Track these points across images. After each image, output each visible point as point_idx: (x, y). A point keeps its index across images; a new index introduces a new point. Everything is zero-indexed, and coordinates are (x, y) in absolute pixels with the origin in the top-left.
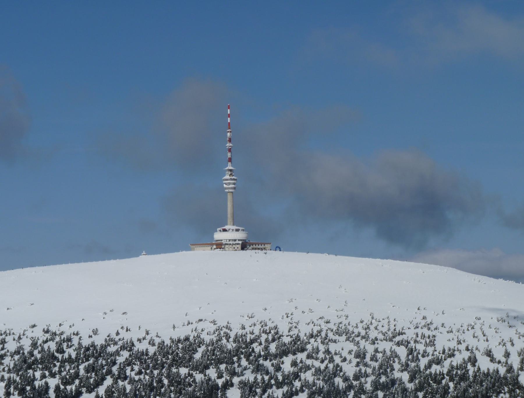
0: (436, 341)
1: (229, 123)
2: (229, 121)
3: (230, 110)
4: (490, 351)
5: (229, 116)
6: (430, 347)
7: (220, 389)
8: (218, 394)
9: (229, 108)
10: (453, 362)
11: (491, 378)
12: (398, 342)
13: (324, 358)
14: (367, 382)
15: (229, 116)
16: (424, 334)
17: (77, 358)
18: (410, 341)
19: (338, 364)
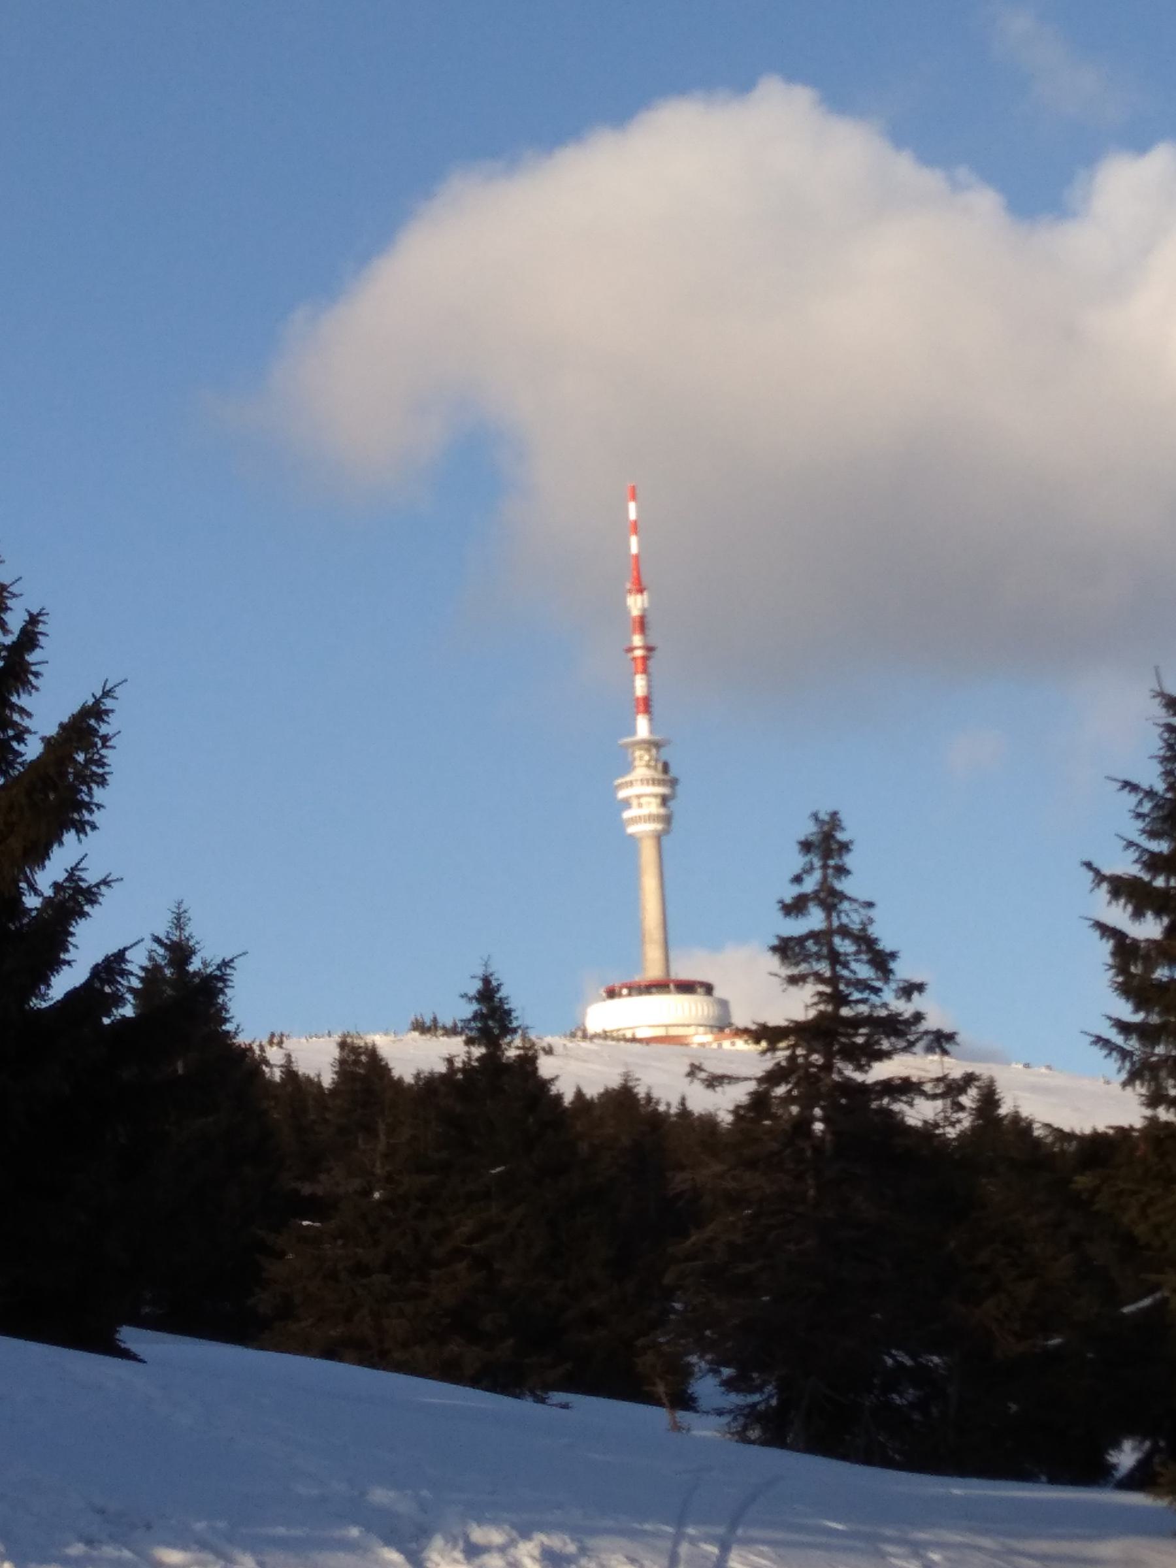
0: (85, 922)
1: (637, 557)
2: (634, 549)
3: (629, 548)
4: (1158, 667)
5: (635, 527)
6: (99, 794)
7: (849, 1040)
8: (494, 1169)
9: (634, 497)
10: (788, 901)
11: (797, 944)
12: (738, 1390)
13: (828, 990)
14: (110, 886)
15: (635, 527)
16: (638, 1085)
17: (833, 981)
18: (268, 1049)
19: (923, 1018)
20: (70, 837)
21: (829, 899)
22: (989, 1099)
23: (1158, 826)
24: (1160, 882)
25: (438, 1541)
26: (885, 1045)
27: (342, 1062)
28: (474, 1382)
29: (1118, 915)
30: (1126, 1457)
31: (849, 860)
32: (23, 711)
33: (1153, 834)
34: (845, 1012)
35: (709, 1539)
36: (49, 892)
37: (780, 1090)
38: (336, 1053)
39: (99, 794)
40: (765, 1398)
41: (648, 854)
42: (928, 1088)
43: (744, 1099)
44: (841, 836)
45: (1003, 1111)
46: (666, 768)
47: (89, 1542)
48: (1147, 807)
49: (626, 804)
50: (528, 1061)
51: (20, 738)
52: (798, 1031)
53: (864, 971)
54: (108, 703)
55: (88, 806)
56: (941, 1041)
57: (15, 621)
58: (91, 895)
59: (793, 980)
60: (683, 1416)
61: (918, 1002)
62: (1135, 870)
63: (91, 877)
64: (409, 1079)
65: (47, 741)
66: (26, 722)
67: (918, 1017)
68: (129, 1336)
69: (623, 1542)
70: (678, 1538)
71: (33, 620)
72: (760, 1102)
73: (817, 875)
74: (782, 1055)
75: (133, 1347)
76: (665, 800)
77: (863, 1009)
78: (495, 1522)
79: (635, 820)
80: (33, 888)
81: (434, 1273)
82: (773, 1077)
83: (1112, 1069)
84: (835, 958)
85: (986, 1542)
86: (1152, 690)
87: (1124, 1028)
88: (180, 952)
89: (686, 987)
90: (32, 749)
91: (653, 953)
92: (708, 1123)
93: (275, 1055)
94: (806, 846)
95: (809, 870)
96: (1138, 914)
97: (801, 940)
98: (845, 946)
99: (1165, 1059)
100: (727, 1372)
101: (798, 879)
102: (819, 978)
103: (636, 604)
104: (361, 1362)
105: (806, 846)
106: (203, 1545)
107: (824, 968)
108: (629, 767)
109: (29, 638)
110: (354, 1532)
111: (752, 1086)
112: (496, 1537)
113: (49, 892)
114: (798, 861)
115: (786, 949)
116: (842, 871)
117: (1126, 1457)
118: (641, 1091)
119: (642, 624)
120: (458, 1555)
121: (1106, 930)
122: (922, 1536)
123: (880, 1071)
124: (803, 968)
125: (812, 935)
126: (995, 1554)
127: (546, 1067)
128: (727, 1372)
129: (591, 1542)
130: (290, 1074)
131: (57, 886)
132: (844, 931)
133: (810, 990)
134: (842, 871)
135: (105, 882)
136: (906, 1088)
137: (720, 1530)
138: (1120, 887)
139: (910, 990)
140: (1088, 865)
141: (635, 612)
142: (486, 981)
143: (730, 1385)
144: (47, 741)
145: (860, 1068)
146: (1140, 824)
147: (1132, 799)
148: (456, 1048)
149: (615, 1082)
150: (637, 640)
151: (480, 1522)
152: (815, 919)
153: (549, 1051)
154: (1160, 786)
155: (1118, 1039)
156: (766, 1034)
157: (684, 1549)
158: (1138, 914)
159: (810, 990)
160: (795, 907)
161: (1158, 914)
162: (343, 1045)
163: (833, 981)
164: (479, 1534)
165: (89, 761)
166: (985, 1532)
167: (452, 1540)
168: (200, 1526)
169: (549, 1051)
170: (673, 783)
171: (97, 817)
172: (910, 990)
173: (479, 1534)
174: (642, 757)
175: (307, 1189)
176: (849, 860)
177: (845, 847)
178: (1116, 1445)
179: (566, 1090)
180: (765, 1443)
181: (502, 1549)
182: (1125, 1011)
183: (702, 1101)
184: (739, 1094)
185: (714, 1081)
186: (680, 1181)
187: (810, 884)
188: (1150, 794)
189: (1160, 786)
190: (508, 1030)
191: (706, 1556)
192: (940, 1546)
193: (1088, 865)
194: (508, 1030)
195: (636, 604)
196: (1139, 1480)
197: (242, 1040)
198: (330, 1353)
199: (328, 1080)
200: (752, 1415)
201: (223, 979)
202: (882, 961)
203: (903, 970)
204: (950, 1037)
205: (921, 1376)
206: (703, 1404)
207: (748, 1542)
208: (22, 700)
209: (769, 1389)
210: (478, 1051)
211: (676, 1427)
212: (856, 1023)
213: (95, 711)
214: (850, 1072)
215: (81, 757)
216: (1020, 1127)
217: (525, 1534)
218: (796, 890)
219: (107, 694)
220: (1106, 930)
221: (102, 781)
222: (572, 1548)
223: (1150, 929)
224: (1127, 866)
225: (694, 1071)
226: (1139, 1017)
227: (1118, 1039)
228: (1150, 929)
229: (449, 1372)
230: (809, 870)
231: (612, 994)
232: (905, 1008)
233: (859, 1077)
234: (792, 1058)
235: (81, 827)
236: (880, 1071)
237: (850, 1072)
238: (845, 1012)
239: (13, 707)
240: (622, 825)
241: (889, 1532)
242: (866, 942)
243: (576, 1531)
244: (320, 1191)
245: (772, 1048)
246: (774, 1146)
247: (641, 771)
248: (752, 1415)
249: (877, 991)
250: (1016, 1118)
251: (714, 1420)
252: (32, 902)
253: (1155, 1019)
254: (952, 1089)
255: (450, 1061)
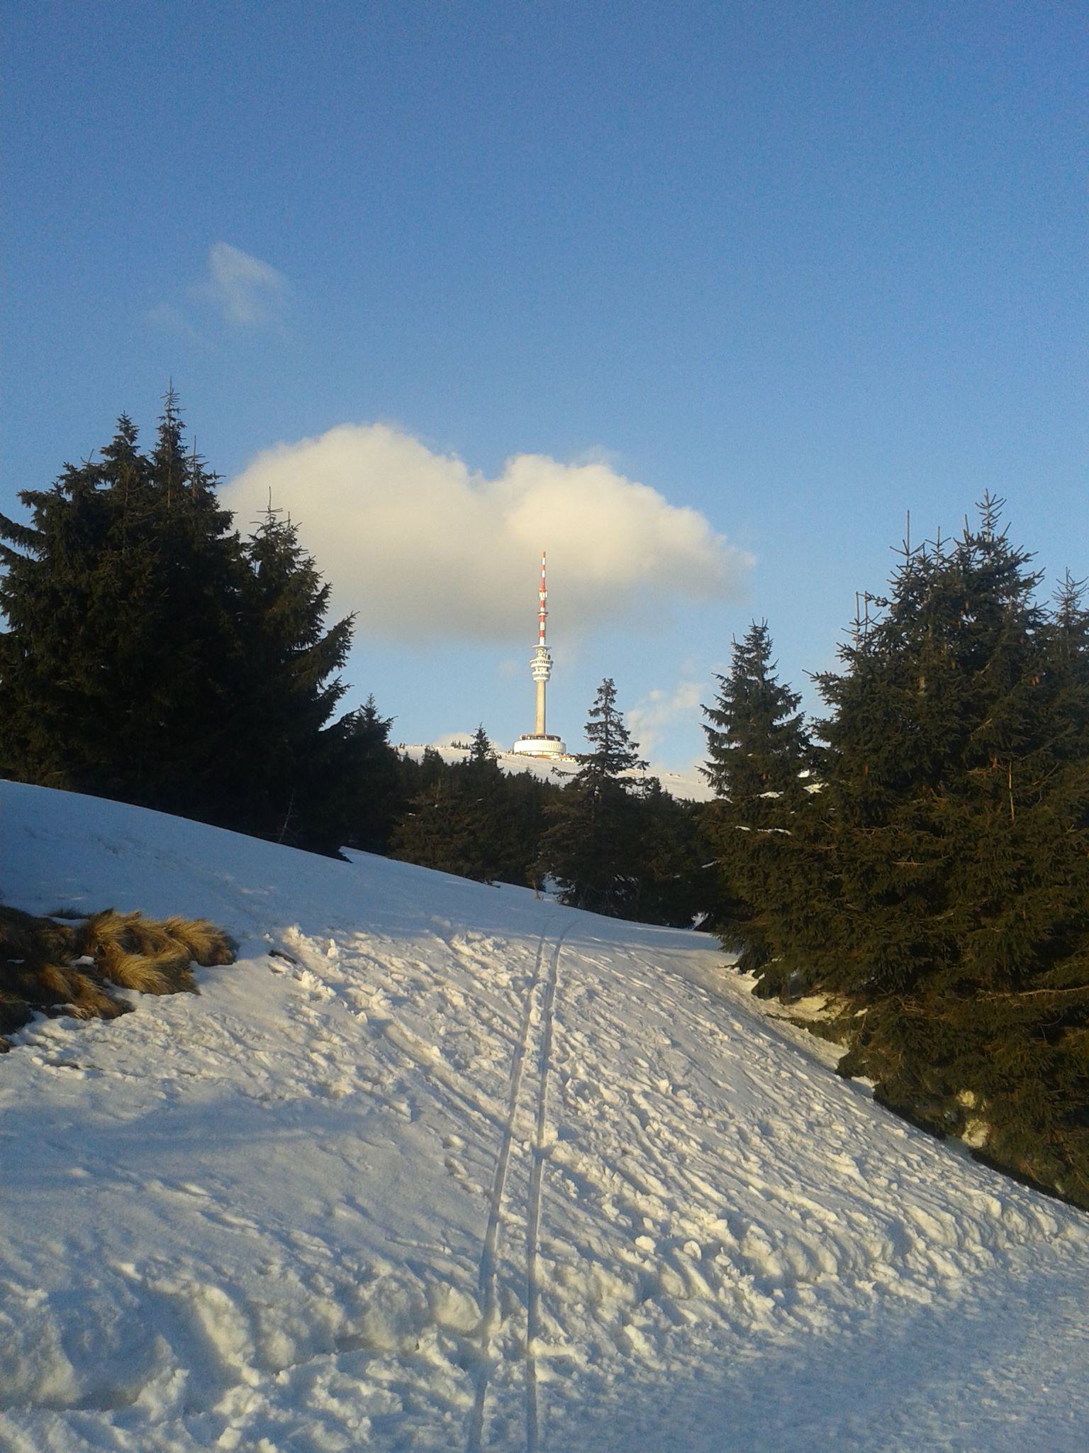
6: (347, 653)
17: (606, 740)
20: (336, 668)
21: (607, 710)
22: (658, 787)
23: (729, 692)
24: (728, 713)
25: (457, 937)
26: (624, 765)
27: (426, 756)
28: (467, 876)
29: (713, 724)
30: (699, 919)
31: (615, 697)
32: (321, 620)
33: (727, 695)
34: (610, 752)
35: (552, 942)
36: (327, 688)
37: (584, 779)
38: (424, 752)
39: (347, 653)
40: (572, 889)
41: (541, 687)
42: (638, 781)
43: (570, 781)
44: (613, 688)
45: (662, 791)
46: (549, 657)
47: (332, 928)
48: (726, 685)
49: (534, 669)
50: (494, 761)
51: (319, 631)
52: (593, 758)
53: (618, 738)
54: (352, 620)
55: (343, 657)
56: (644, 765)
57: (320, 587)
58: (342, 691)
59: (592, 739)
60: (541, 893)
61: (636, 751)
62: (719, 708)
63: (343, 684)
64: (450, 764)
65: (329, 632)
66: (322, 625)
67: (636, 756)
68: (344, 850)
69: (521, 941)
70: (541, 942)
71: (327, 587)
72: (576, 783)
73: (604, 701)
74: (586, 765)
75: (346, 855)
76: (548, 669)
77: (616, 751)
78: (477, 931)
79: (537, 675)
80: (321, 686)
81: (455, 836)
82: (582, 774)
83: (705, 781)
84: (607, 732)
85: (650, 949)
86: (68, 467)
87: (710, 765)
88: (371, 712)
89: (551, 738)
90: (323, 635)
91: (540, 724)
92: (556, 787)
93: (401, 751)
94: (600, 691)
95: (601, 699)
96: (719, 724)
97: (596, 725)
98: (612, 728)
99: (725, 777)
100: (558, 879)
101: (596, 703)
102: (601, 739)
103: (542, 596)
104: (426, 866)
105: (600, 691)
106: (373, 932)
107: (603, 735)
108: (537, 656)
109: (325, 593)
110: (427, 931)
111: (573, 777)
112: (478, 937)
113: (327, 688)
114: (598, 696)
115: (590, 728)
116: (612, 701)
117: (699, 919)
118: (533, 775)
119: (544, 604)
120: (464, 942)
121: (707, 728)
122: (626, 945)
123: (621, 774)
124: (596, 735)
125: (599, 723)
126: (654, 953)
127: (500, 764)
128: (558, 879)
129: (511, 940)
130: (407, 758)
131: (330, 686)
132: (612, 723)
133: (598, 743)
134: (612, 701)
135: (348, 686)
136: (630, 781)
137: (557, 939)
138: (714, 714)
139: (634, 746)
140: (703, 706)
141: (542, 599)
142: (480, 731)
143: (559, 883)
144: (329, 632)
145: (614, 773)
146: (723, 691)
147: (721, 682)
148: (467, 753)
149: (524, 771)
150: (542, 609)
151: (472, 930)
152: (601, 718)
153: (500, 758)
154: (731, 678)
155: (709, 770)
156: (581, 759)
157: (544, 945)
158: (719, 724)
159: (598, 743)
160: (594, 713)
161: (727, 724)
162: (426, 750)
163: (606, 740)
164: (471, 935)
165: (344, 641)
166: (650, 945)
167: (461, 937)
168: (372, 925)
169: (500, 758)
170: (552, 662)
171: (345, 662)
172: (634, 746)
173: (471, 935)
174: (541, 653)
175: (411, 802)
176: (615, 697)
177: (614, 692)
178: (696, 914)
179: (505, 772)
180: (568, 905)
181: (480, 941)
182: (712, 760)
183: (554, 779)
184: (569, 779)
185: (561, 774)
186: (547, 809)
187: (600, 705)
188: (727, 680)
189: (731, 678)
190: (486, 749)
191: (551, 948)
192: (634, 949)
193: (703, 706)
194: (486, 749)
195: (542, 596)
196: (701, 928)
197: (392, 745)
198: (416, 862)
199: (420, 762)
200: (566, 895)
201: (388, 725)
202: (624, 735)
203: (631, 738)
204: (647, 764)
205: (627, 885)
206: (547, 889)
207: (566, 944)
208: (321, 616)
209: (573, 886)
210: (475, 756)
211: (539, 897)
212: (614, 756)
213: (347, 622)
214: (610, 774)
215: (341, 639)
216: (668, 797)
217: (488, 937)
218: (595, 706)
219: (352, 616)
220: (707, 728)
221: (349, 649)
222: (504, 943)
223: (723, 729)
224: (717, 707)
225: (554, 769)
226: (717, 762)
227: (709, 770)
228: (723, 729)
229: (458, 872)
230: (601, 699)
231: (524, 738)
232: (632, 753)
233: (613, 776)
234: (590, 767)
235: (340, 665)
236: (621, 774)
237: (610, 774)
238: (610, 752)
239: (317, 618)
240: (532, 677)
241: (617, 943)
242: (619, 727)
243: (505, 937)
244: (416, 802)
245: (583, 763)
246: (581, 799)
247: (540, 658)
248: (566, 895)
249: (622, 745)
250: (666, 793)
251: (552, 895)
252: (320, 691)
253: (723, 763)
254: (646, 782)
255: (465, 759)
